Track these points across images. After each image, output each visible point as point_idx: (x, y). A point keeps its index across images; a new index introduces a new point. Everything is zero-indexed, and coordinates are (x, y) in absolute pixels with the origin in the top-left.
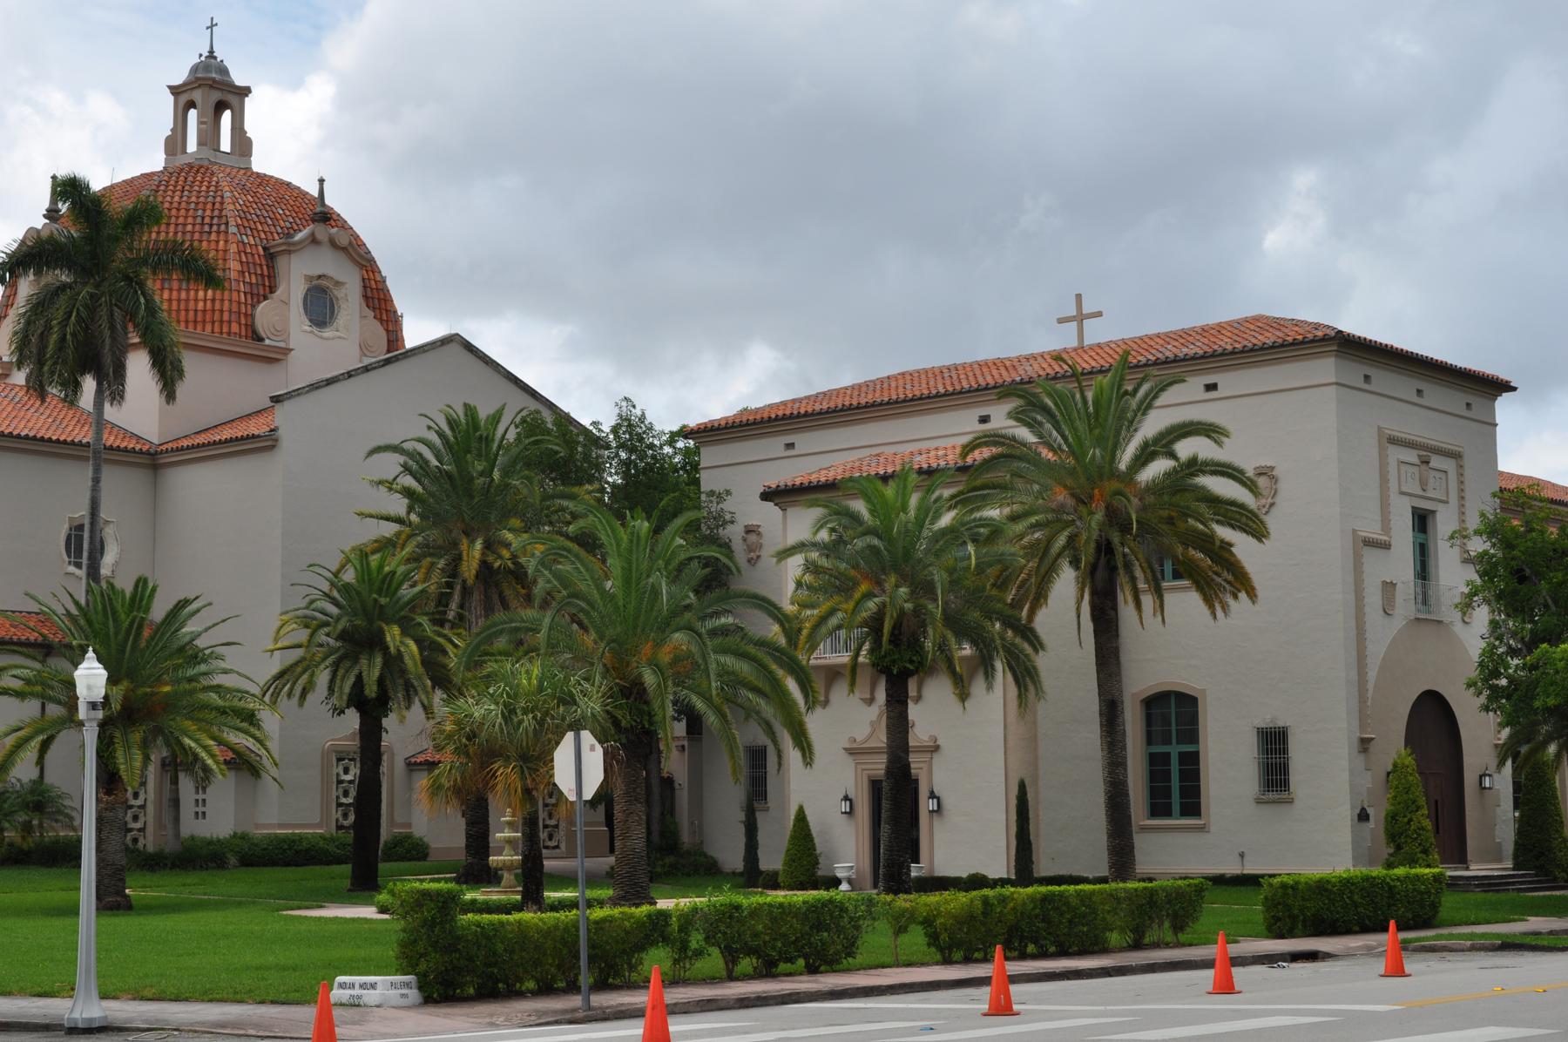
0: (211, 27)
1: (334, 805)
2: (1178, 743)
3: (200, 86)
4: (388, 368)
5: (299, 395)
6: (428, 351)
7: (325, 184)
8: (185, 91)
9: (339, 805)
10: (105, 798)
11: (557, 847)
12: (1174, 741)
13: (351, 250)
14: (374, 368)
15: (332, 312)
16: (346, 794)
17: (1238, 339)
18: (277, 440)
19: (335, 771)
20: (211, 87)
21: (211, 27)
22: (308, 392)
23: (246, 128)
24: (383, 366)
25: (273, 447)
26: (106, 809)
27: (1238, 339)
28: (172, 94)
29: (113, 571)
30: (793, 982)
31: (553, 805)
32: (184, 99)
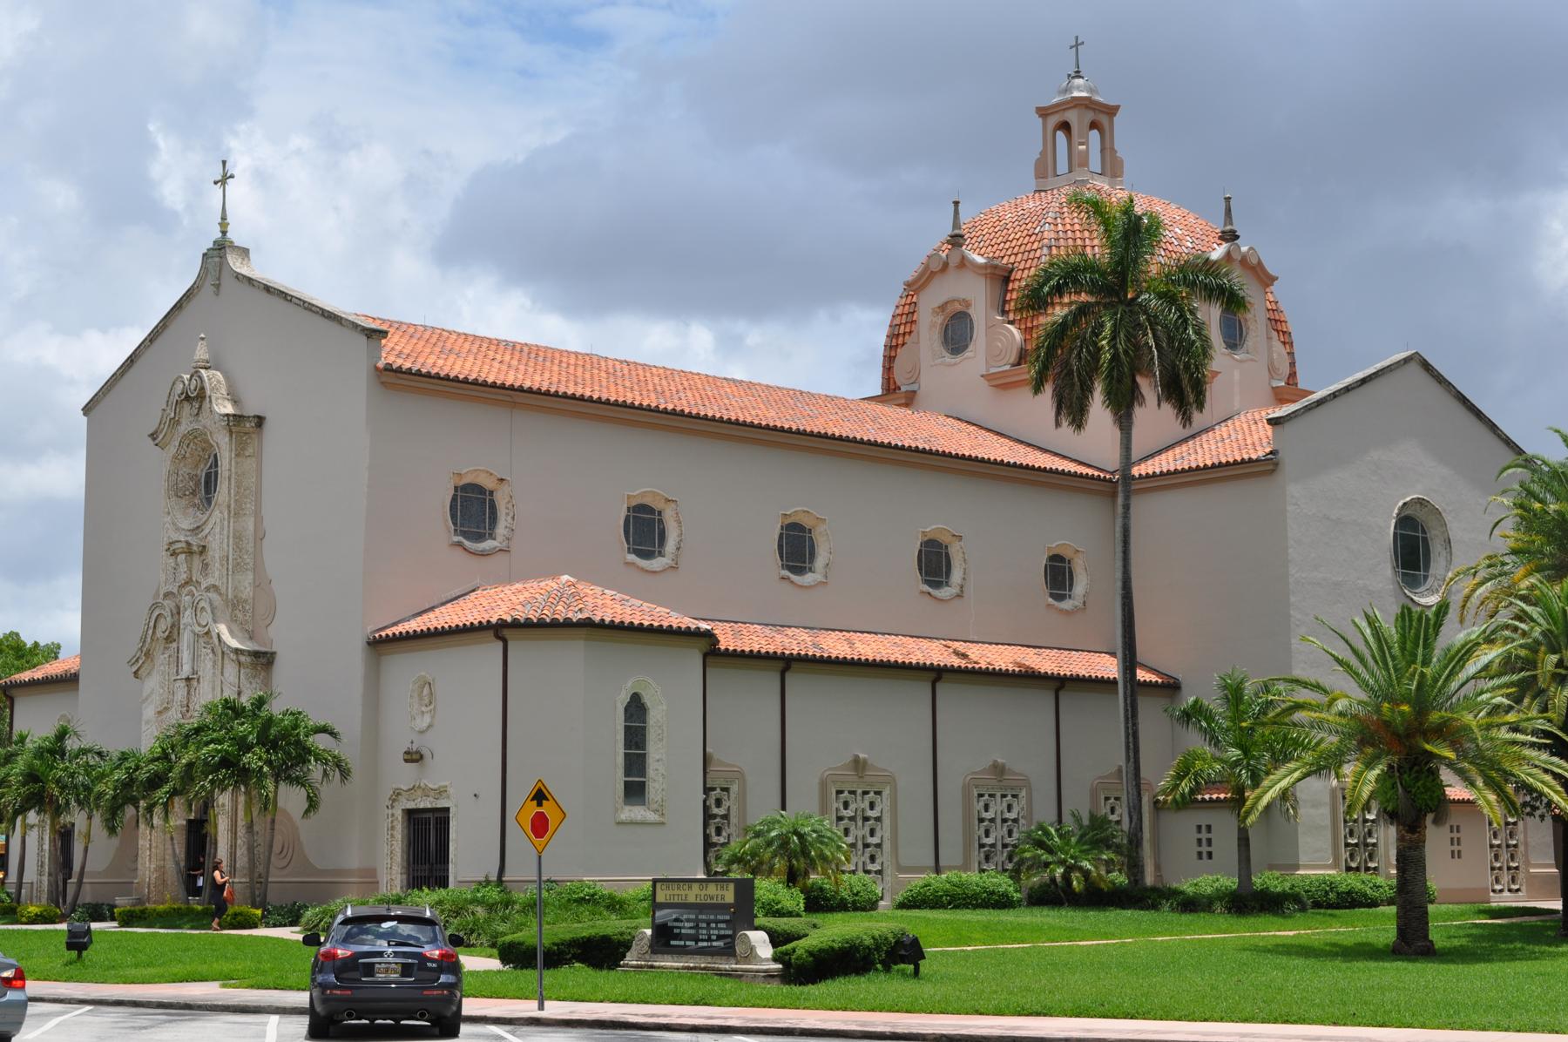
0: (1077, 45)
1: (977, 846)
2: (625, 782)
3: (1075, 106)
4: (1365, 386)
5: (1296, 416)
6: (1394, 369)
7: (1232, 202)
8: (1056, 112)
9: (1347, 845)
10: (1408, 836)
11: (1518, 890)
12: (627, 779)
13: (1258, 269)
14: (1353, 388)
15: (1241, 335)
16: (1351, 834)
17: (588, 382)
18: (1276, 464)
19: (835, 805)
20: (1087, 107)
21: (1077, 45)
22: (1303, 413)
23: (1116, 148)
24: (1360, 386)
25: (1273, 471)
26: (1410, 848)
27: (588, 382)
28: (1040, 116)
29: (1084, 602)
30: (1120, 1031)
31: (723, 845)
32: (1053, 120)
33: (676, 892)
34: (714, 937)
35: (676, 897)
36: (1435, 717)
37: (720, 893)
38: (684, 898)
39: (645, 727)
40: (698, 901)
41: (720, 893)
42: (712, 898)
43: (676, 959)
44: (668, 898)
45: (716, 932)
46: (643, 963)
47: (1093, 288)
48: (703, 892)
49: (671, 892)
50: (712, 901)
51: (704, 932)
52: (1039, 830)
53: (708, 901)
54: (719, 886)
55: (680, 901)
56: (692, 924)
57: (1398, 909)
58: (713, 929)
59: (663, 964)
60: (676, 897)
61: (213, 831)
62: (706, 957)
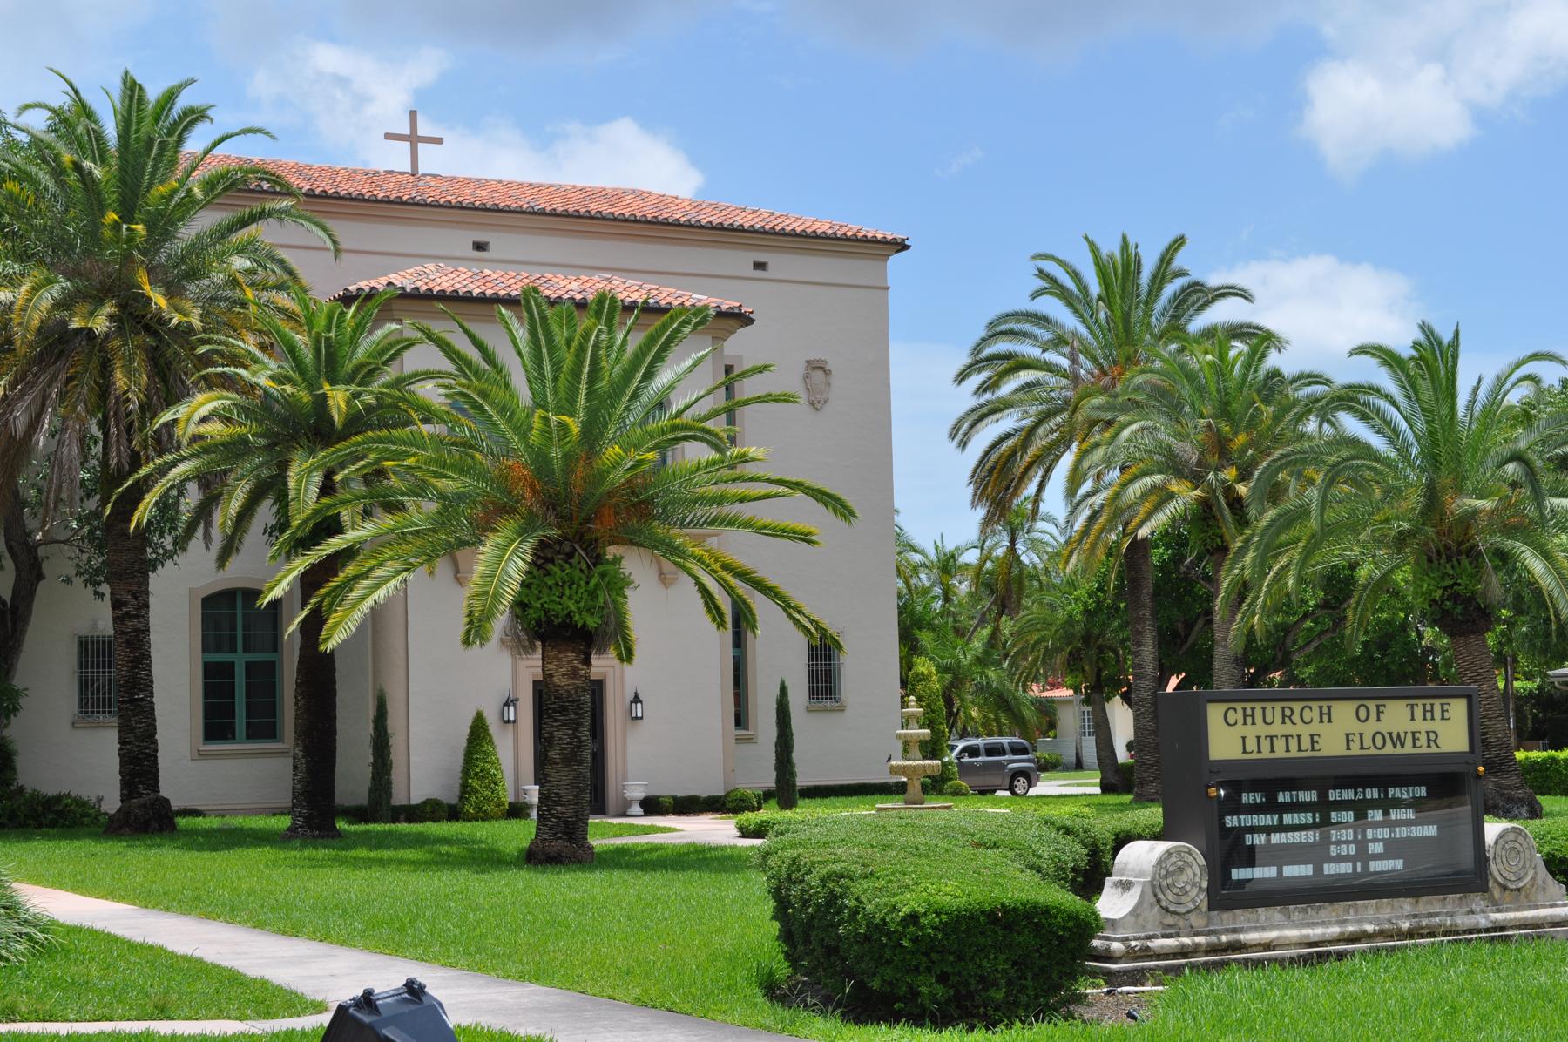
33: (1278, 728)
34: (1378, 848)
35: (1280, 745)
36: (1000, 586)
37: (1421, 725)
38: (1306, 744)
39: (205, 650)
40: (1355, 750)
41: (1421, 725)
42: (1398, 740)
43: (1297, 916)
44: (1251, 745)
45: (1383, 833)
46: (1186, 941)
47: (143, 534)
48: (1370, 728)
49: (1261, 729)
50: (1399, 750)
51: (1348, 834)
52: (1282, 630)
53: (1389, 749)
54: (1419, 712)
55: (1294, 753)
56: (1306, 818)
57: (794, 782)
58: (1376, 825)
59: (1272, 935)
60: (1280, 745)
61: (446, 186)
62: (1396, 902)
